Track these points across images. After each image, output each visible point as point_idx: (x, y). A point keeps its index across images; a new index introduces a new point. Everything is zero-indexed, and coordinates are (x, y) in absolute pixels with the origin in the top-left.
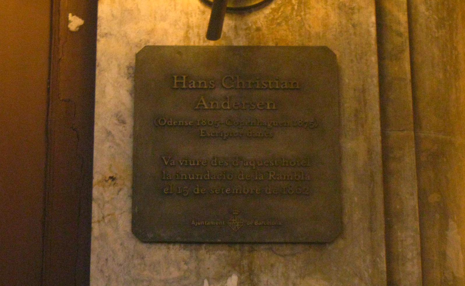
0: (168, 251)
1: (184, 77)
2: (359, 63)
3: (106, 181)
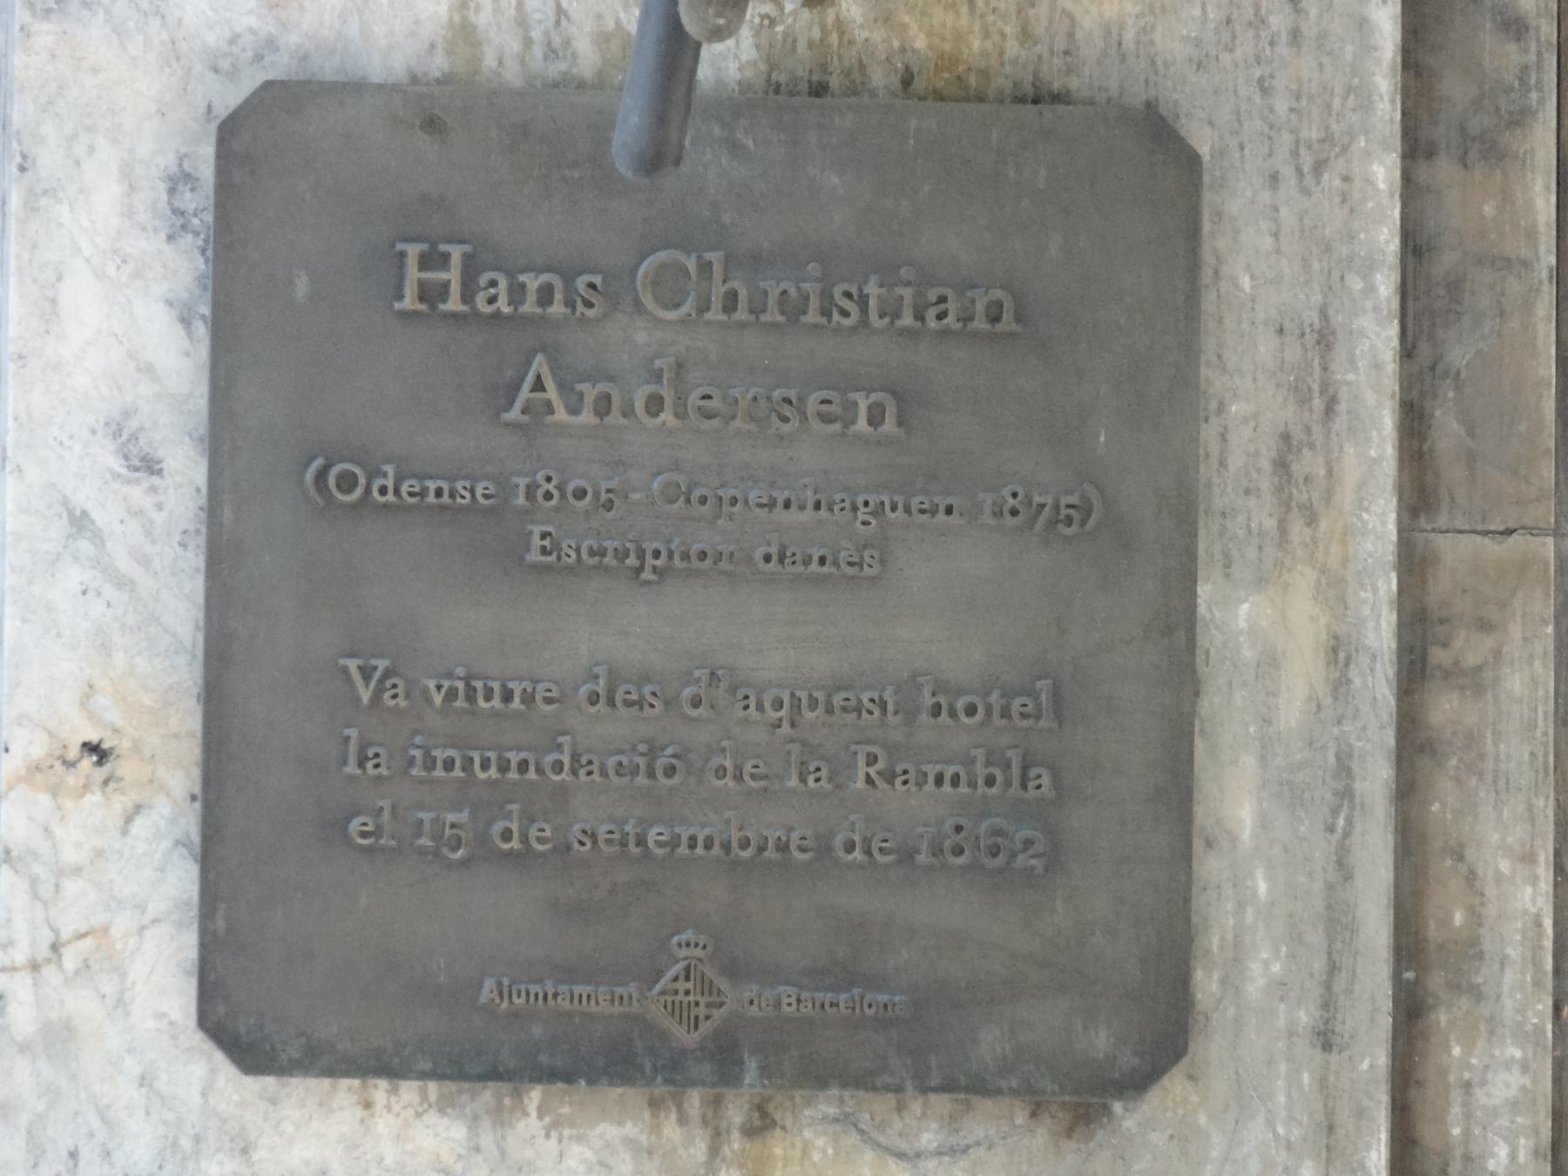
0: (362, 1121)
1: (456, 252)
2: (1306, 192)
3: (69, 764)
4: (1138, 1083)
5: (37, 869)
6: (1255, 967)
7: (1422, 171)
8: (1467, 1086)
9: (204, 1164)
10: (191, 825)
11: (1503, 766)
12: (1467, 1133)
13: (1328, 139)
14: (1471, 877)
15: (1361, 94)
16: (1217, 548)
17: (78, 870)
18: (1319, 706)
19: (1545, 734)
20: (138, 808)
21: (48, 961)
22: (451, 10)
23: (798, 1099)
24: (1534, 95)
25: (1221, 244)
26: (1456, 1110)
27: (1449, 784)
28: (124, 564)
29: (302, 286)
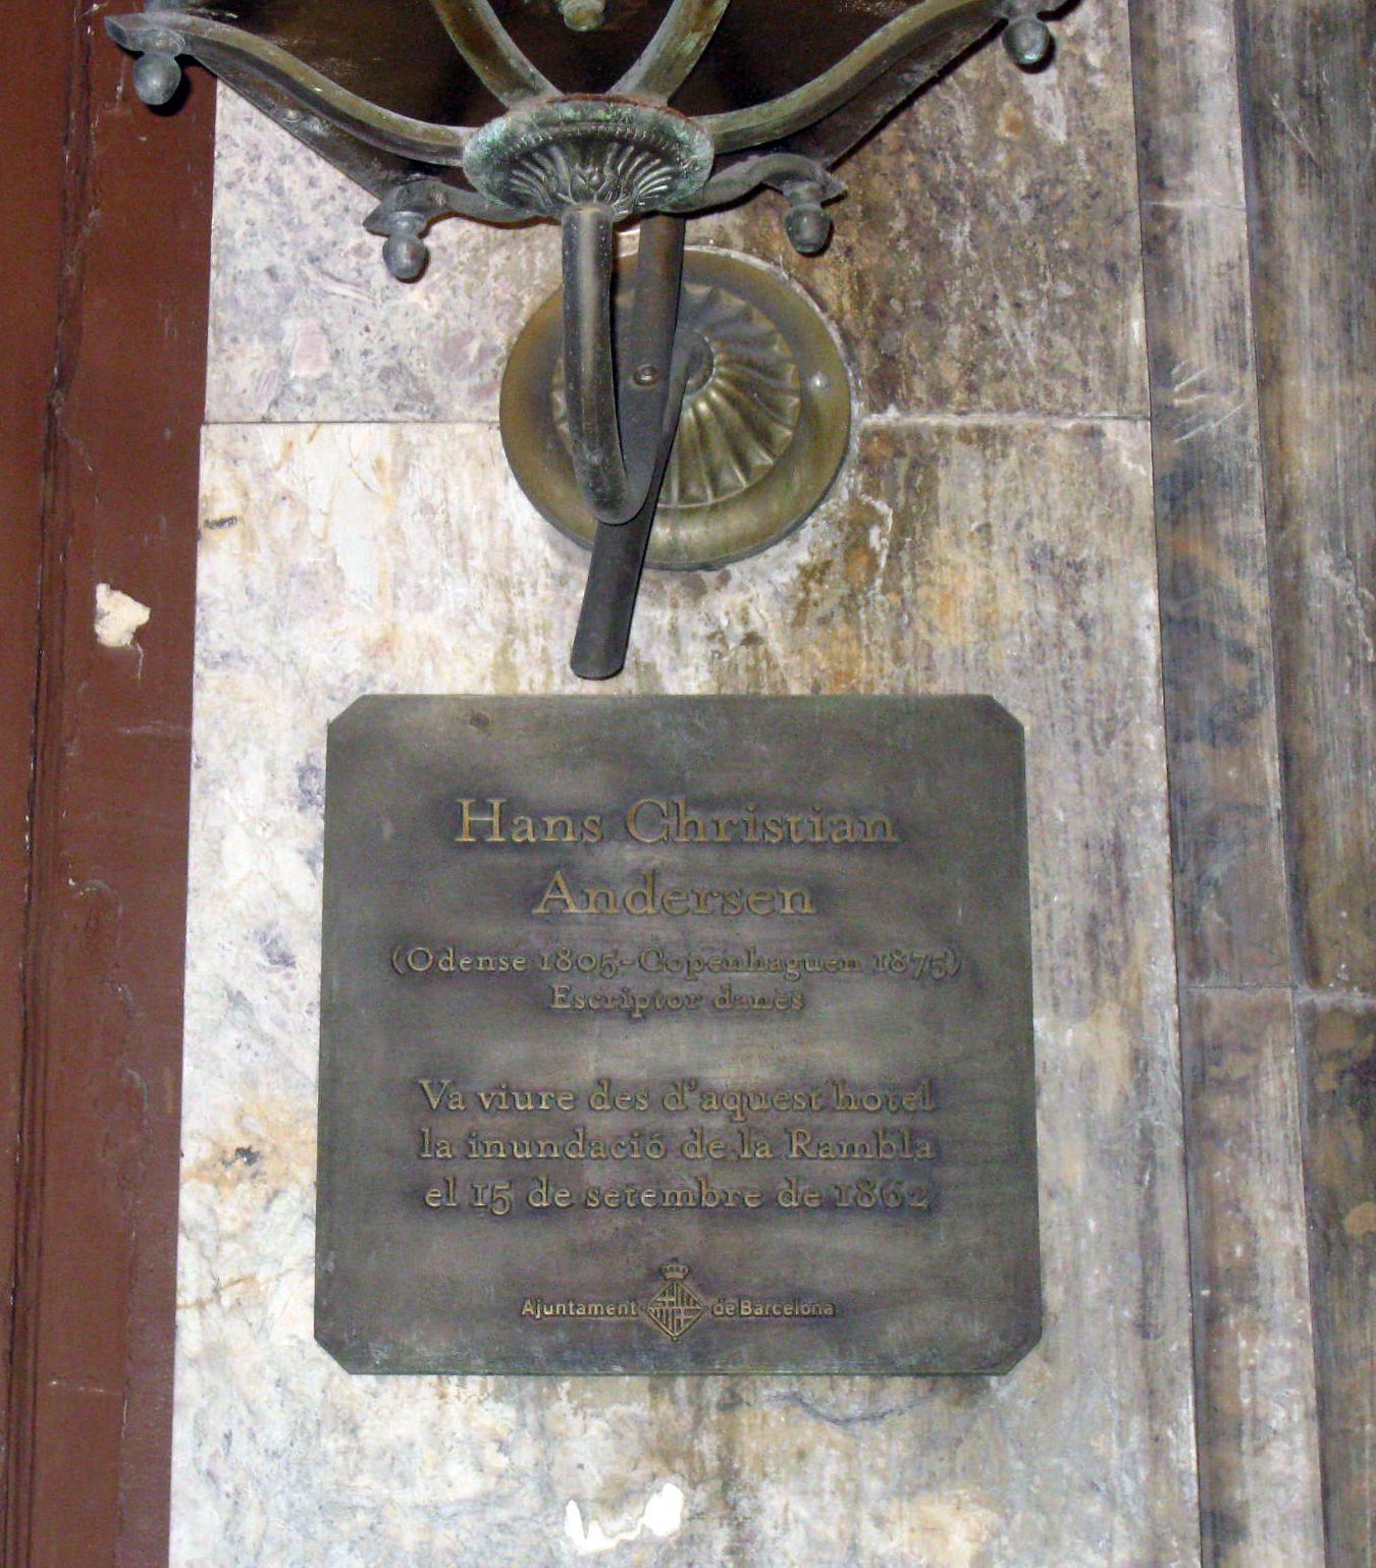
0: (439, 1408)
2: (1099, 753)
4: (1005, 1361)
5: (203, 1236)
6: (1091, 1281)
7: (1184, 750)
8: (1252, 1369)
9: (323, 1440)
10: (311, 1203)
11: (1264, 1145)
12: (1254, 1403)
13: (1113, 718)
14: (1247, 1224)
15: (1134, 688)
16: (1048, 993)
17: (233, 1237)
18: (1127, 1099)
19: (1294, 1122)
20: (276, 1193)
21: (211, 1300)
22: (496, 654)
23: (758, 1383)
24: (1260, 698)
25: (1042, 789)
26: (1244, 1387)
27: (1227, 1159)
28: (267, 1026)
29: (388, 831)
